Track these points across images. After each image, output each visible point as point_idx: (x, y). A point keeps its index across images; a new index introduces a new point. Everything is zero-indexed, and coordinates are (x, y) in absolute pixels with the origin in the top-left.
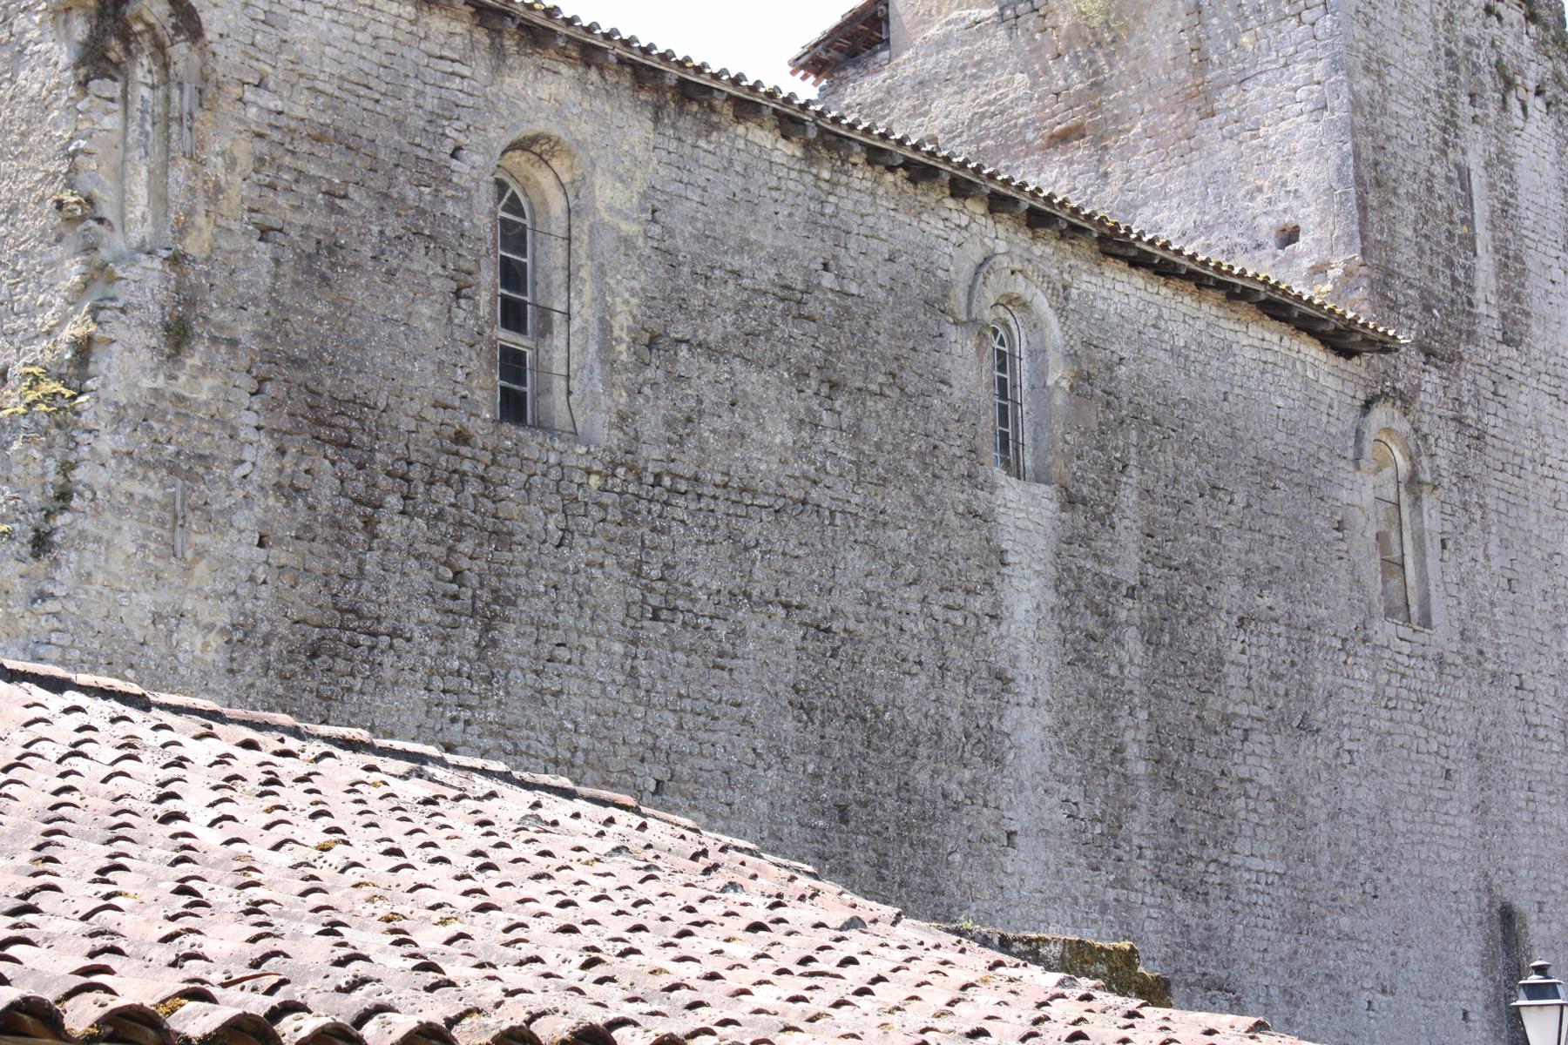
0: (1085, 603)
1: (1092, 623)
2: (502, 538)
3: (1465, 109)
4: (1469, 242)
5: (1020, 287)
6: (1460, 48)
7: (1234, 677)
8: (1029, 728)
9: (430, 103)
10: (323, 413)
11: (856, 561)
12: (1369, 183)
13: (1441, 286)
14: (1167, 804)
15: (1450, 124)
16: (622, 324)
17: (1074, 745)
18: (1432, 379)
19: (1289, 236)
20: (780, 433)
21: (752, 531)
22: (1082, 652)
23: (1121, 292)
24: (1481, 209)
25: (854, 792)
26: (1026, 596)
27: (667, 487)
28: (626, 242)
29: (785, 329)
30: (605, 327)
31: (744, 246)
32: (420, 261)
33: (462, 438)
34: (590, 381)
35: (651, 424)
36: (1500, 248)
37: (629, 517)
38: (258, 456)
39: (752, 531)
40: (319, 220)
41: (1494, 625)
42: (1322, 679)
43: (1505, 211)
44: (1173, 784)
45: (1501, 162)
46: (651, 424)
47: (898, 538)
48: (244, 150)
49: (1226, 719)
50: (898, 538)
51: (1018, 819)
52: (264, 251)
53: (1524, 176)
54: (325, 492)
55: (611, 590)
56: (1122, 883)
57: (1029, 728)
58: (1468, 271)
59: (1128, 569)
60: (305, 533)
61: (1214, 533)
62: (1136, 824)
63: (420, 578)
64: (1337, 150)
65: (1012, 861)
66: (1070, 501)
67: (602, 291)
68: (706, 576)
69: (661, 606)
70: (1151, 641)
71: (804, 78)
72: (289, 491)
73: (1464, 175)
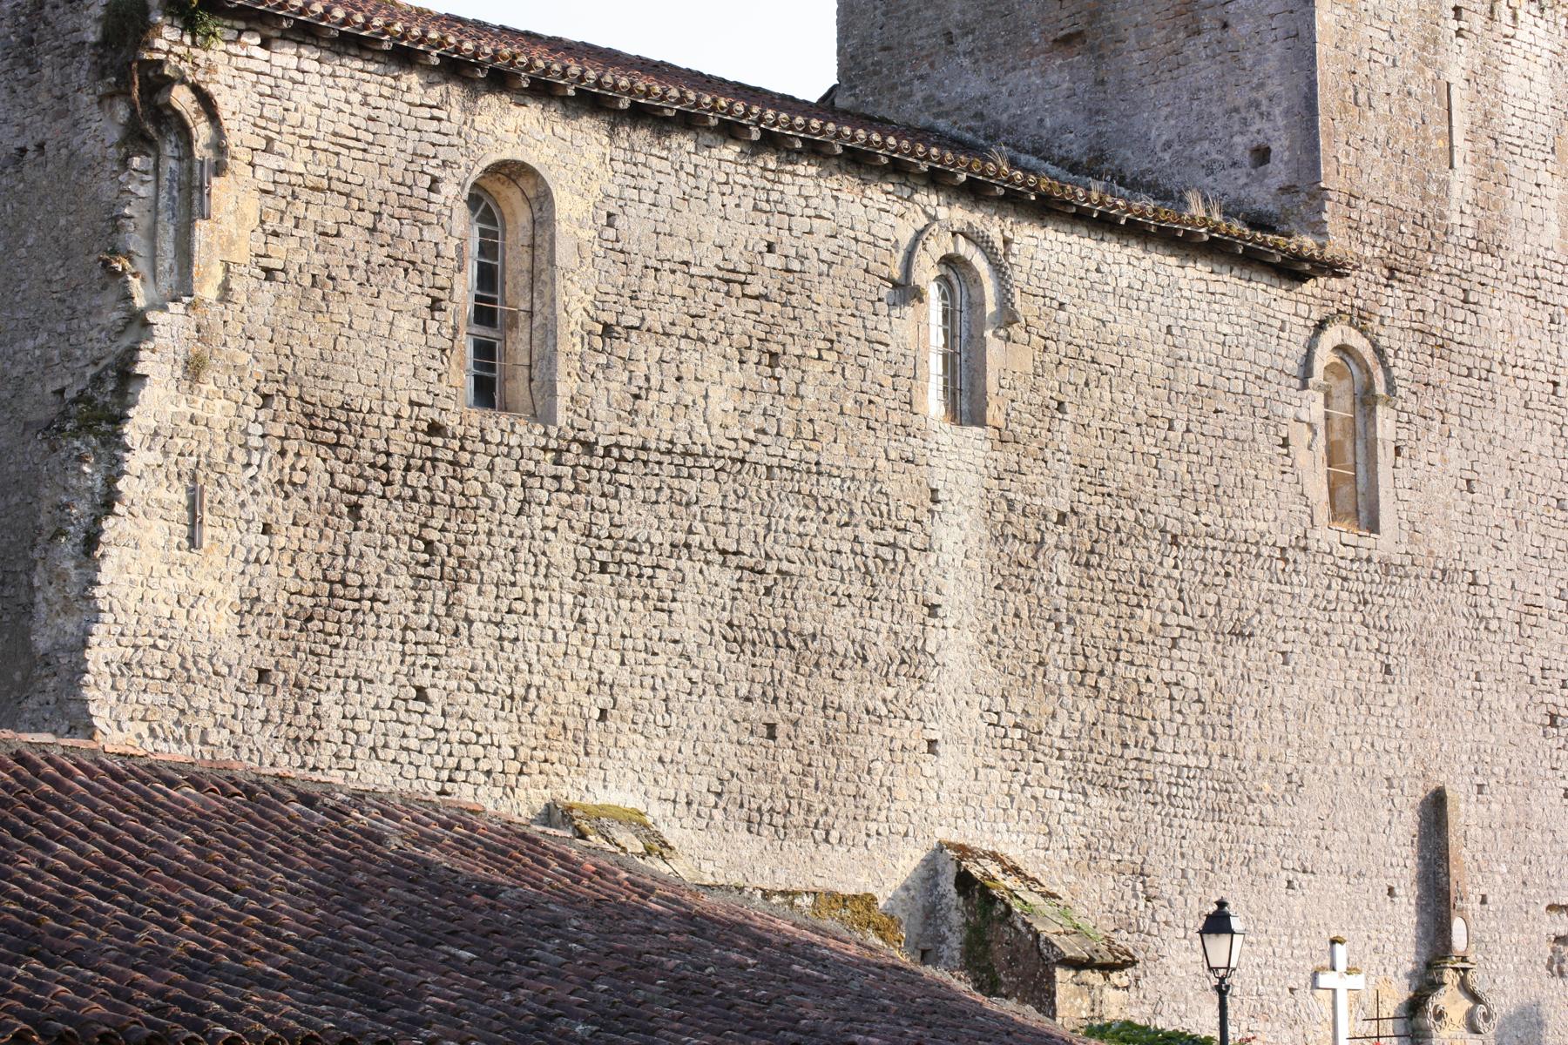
19: (1262, 155)
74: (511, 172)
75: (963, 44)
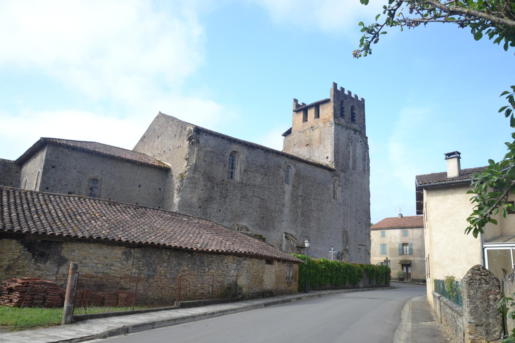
0: (294, 197)
1: (295, 199)
2: (227, 190)
3: (350, 144)
4: (349, 159)
5: (290, 164)
6: (350, 137)
7: (313, 205)
8: (286, 210)
9: (223, 148)
10: (209, 178)
11: (267, 192)
12: (336, 152)
13: (345, 164)
14: (303, 218)
15: (348, 146)
16: (242, 170)
17: (292, 212)
18: (342, 174)
19: (327, 158)
20: (259, 180)
21: (256, 190)
22: (294, 202)
23: (302, 165)
24: (351, 155)
25: (265, 216)
26: (287, 196)
27: (246, 185)
28: (244, 161)
29: (261, 169)
30: (240, 170)
31: (257, 161)
32: (221, 163)
33: (224, 180)
34: (238, 175)
35: (245, 179)
36: (353, 159)
37: (242, 188)
38: (202, 183)
39: (256, 190)
40: (210, 160)
41: (348, 200)
42: (324, 206)
43: (354, 156)
44: (303, 216)
45: (355, 150)
46: (245, 179)
47: (273, 190)
48: (203, 153)
49: (311, 210)
50: (273, 190)
51: (284, 219)
52: (204, 163)
53: (357, 151)
54: (209, 185)
55: (239, 195)
56: (296, 226)
57: (286, 210)
58: (349, 162)
59: (300, 193)
60: (206, 189)
61: (312, 190)
62: (299, 220)
63: (218, 194)
64: (333, 149)
65: (283, 223)
66: (294, 187)
67: (241, 166)
68: (250, 194)
69: (244, 197)
70: (302, 201)
71: (498, 41)
72: (205, 185)
73: (349, 151)
74: (235, 152)
75: (296, 145)
